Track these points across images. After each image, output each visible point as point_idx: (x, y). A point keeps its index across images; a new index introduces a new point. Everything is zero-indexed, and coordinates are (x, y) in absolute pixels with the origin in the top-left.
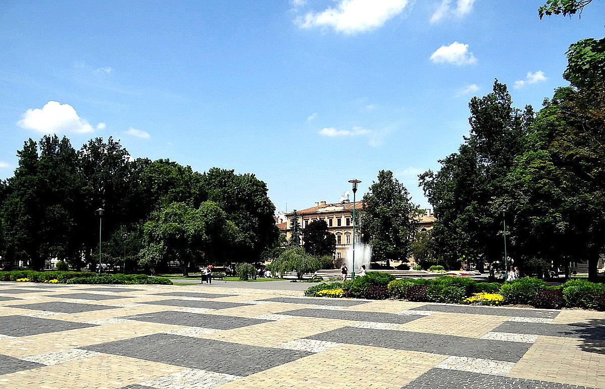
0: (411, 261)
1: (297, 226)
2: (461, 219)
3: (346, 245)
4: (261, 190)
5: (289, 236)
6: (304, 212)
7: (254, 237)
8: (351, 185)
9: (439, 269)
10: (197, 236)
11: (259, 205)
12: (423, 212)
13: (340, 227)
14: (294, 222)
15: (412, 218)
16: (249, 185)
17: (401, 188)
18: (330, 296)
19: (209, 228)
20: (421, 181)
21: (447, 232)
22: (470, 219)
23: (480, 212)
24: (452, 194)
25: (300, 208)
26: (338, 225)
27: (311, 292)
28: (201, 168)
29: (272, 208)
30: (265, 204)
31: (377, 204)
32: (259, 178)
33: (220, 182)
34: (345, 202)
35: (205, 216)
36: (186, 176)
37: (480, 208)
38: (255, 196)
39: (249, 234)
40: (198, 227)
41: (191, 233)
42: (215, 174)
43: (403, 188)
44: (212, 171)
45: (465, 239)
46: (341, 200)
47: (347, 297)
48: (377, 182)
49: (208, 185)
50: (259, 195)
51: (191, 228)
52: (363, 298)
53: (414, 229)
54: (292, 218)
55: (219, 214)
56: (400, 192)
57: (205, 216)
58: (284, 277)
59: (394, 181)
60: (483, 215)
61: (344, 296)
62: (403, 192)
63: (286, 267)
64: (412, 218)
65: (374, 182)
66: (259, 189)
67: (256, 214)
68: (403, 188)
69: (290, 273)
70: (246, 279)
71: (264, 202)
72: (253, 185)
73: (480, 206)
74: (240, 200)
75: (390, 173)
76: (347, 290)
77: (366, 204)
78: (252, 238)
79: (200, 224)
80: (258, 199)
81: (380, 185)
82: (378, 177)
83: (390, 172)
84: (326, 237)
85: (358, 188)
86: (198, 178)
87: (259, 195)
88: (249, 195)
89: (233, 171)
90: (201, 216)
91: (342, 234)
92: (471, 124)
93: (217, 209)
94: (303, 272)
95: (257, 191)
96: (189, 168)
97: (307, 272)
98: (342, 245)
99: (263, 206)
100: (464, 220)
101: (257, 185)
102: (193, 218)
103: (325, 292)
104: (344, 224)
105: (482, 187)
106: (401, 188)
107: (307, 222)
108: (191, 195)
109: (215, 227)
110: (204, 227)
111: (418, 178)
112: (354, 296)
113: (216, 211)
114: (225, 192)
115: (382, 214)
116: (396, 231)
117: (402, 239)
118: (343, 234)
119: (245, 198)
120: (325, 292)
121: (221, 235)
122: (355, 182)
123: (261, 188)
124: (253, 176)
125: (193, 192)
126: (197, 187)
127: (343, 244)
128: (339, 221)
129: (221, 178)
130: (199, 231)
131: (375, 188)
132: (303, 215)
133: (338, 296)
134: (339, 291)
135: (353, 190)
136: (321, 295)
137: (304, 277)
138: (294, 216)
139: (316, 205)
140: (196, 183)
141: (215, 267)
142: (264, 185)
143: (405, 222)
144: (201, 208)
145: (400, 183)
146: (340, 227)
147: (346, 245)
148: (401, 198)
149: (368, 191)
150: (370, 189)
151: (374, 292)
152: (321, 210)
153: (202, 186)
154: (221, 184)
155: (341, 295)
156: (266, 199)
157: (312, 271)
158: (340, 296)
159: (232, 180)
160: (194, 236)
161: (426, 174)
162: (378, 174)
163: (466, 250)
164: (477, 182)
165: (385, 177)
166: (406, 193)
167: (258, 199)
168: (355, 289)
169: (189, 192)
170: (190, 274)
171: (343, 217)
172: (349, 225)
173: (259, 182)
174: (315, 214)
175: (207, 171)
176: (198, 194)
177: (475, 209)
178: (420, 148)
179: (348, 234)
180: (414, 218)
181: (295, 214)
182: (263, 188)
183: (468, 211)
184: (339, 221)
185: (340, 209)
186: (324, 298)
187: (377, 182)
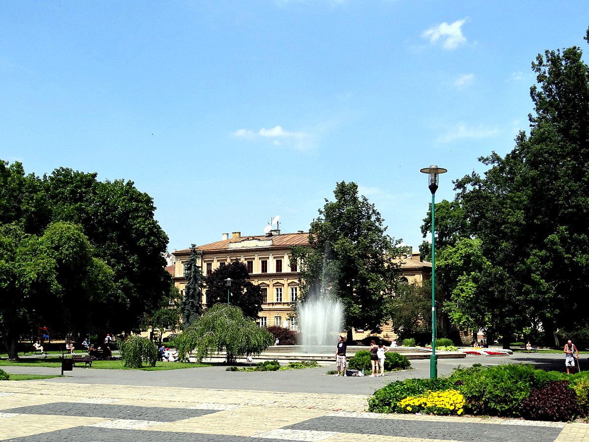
0: (387, 331)
1: (197, 271)
2: (538, 256)
3: (276, 304)
4: (145, 209)
5: (181, 287)
6: (205, 249)
7: (131, 289)
8: (426, 179)
9: (447, 344)
10: (40, 285)
11: (141, 234)
12: (404, 251)
13: (265, 275)
14: (190, 266)
15: (389, 260)
16: (124, 200)
17: (371, 212)
18: (430, 411)
19: (64, 270)
20: (460, 191)
21: (510, 280)
22: (557, 258)
23: (571, 244)
24: (520, 215)
25: (203, 242)
26: (263, 271)
27: (384, 402)
28: (39, 167)
29: (163, 241)
30: (152, 233)
31: (334, 238)
32: (140, 187)
33: (73, 192)
34: (273, 233)
35: (57, 248)
36: (13, 180)
37: (571, 238)
38: (134, 218)
39: (122, 283)
40: (44, 268)
41: (30, 279)
42: (63, 178)
43: (373, 211)
44: (58, 173)
45: (545, 293)
46: (267, 230)
47: (476, 415)
48: (334, 200)
49: (52, 197)
50: (140, 217)
51: (30, 271)
52: (516, 416)
53: (392, 278)
54: (187, 259)
55: (82, 246)
56: (369, 218)
57: (57, 248)
58: (204, 360)
59: (361, 199)
60: (576, 250)
61: (468, 411)
62: (373, 218)
63: (210, 342)
64: (389, 260)
65: (327, 201)
66: (141, 207)
67: (134, 248)
68: (373, 211)
69: (216, 353)
70: (140, 366)
71: (149, 228)
72: (130, 200)
73: (571, 234)
74: (110, 226)
75: (354, 187)
76: (477, 398)
77: (314, 236)
78: (126, 290)
79: (48, 262)
80: (139, 223)
81: (339, 206)
82: (335, 192)
83: (354, 185)
84: (245, 290)
85: (440, 184)
86: (33, 185)
87: (140, 217)
88: (125, 215)
89: (95, 175)
90: (48, 247)
91: (268, 286)
92: (533, 98)
93: (79, 235)
94: (241, 352)
95: (137, 210)
96: (19, 165)
97: (249, 352)
98: (269, 304)
99: (148, 237)
100: (544, 260)
101: (138, 201)
102: (34, 252)
103: (415, 401)
104: (272, 268)
105: (573, 201)
106: (371, 212)
107: (209, 265)
108: (19, 213)
109: (73, 269)
110: (56, 268)
111: (454, 186)
112: (493, 413)
113: (77, 240)
114: (80, 210)
115: (344, 249)
116: (364, 281)
117: (374, 294)
118: (286, 285)
119: (122, 221)
120: (415, 401)
121: (83, 284)
122: (435, 172)
123: (145, 205)
124: (130, 184)
125: (24, 208)
126: (32, 199)
127: (270, 302)
128: (279, 265)
129: (72, 188)
130: (46, 276)
131: (330, 210)
132: (204, 254)
133: (453, 413)
134: (453, 398)
135: (430, 187)
136: (409, 408)
137: (238, 361)
138: (190, 256)
139: (225, 238)
140: (31, 192)
141: (51, 342)
142: (149, 201)
143: (377, 268)
144: (47, 233)
145: (370, 202)
146: (265, 275)
147: (276, 304)
148: (371, 228)
149: (317, 215)
150: (321, 212)
151: (545, 403)
152: (233, 246)
153: (42, 199)
154: (75, 197)
155: (461, 410)
156: (153, 224)
157: (257, 349)
158: (459, 413)
159: (94, 189)
160: (35, 284)
161: (467, 180)
162: (334, 187)
163: (548, 312)
164: (567, 192)
165: (346, 192)
166: (378, 220)
167: (138, 224)
168: (497, 396)
169: (18, 209)
170: (22, 355)
171: (271, 258)
172: (281, 271)
173: (140, 194)
174: (226, 252)
175: (50, 174)
176: (32, 213)
177: (563, 240)
178: (439, 135)
179: (279, 288)
180: (393, 261)
181: (194, 251)
182: (147, 205)
183: (553, 243)
184: (279, 265)
185: (267, 244)
186: (419, 417)
187: (334, 200)
